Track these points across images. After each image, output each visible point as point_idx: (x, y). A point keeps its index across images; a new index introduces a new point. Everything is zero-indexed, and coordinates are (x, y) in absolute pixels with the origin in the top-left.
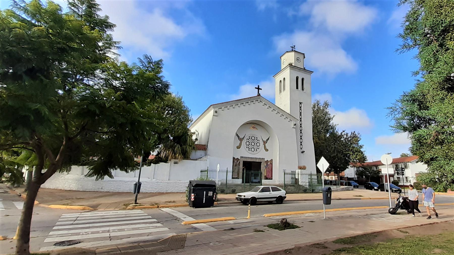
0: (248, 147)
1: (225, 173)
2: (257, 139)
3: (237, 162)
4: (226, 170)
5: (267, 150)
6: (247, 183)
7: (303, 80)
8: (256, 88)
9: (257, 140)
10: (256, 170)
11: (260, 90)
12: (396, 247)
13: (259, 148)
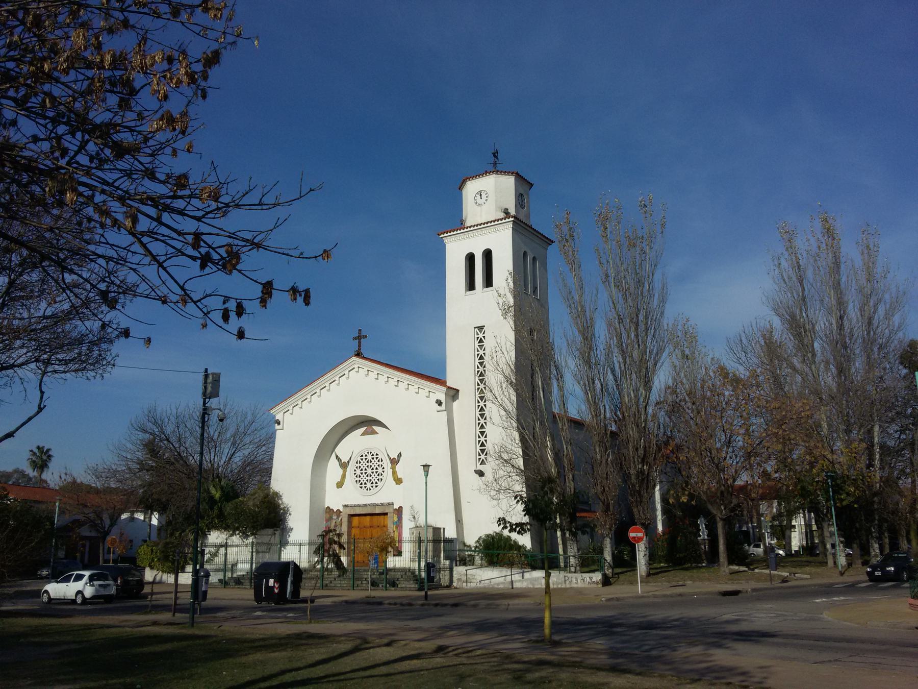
3: (338, 518)
5: (398, 481)
8: (360, 331)
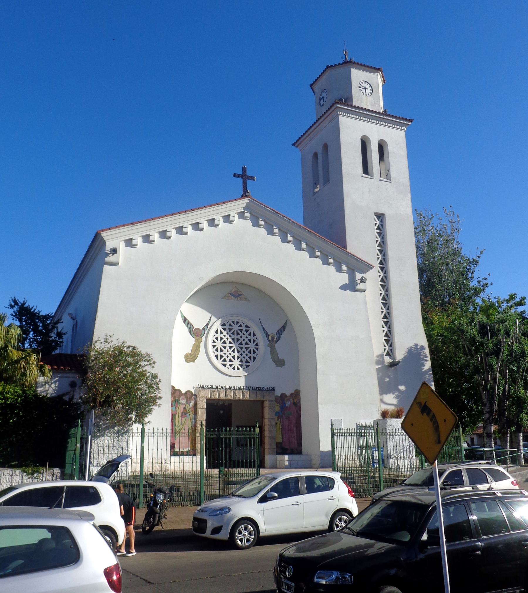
2: (247, 331)
5: (280, 363)
7: (382, 147)
8: (235, 175)
9: (246, 334)
10: (242, 427)
11: (248, 181)
13: (255, 358)
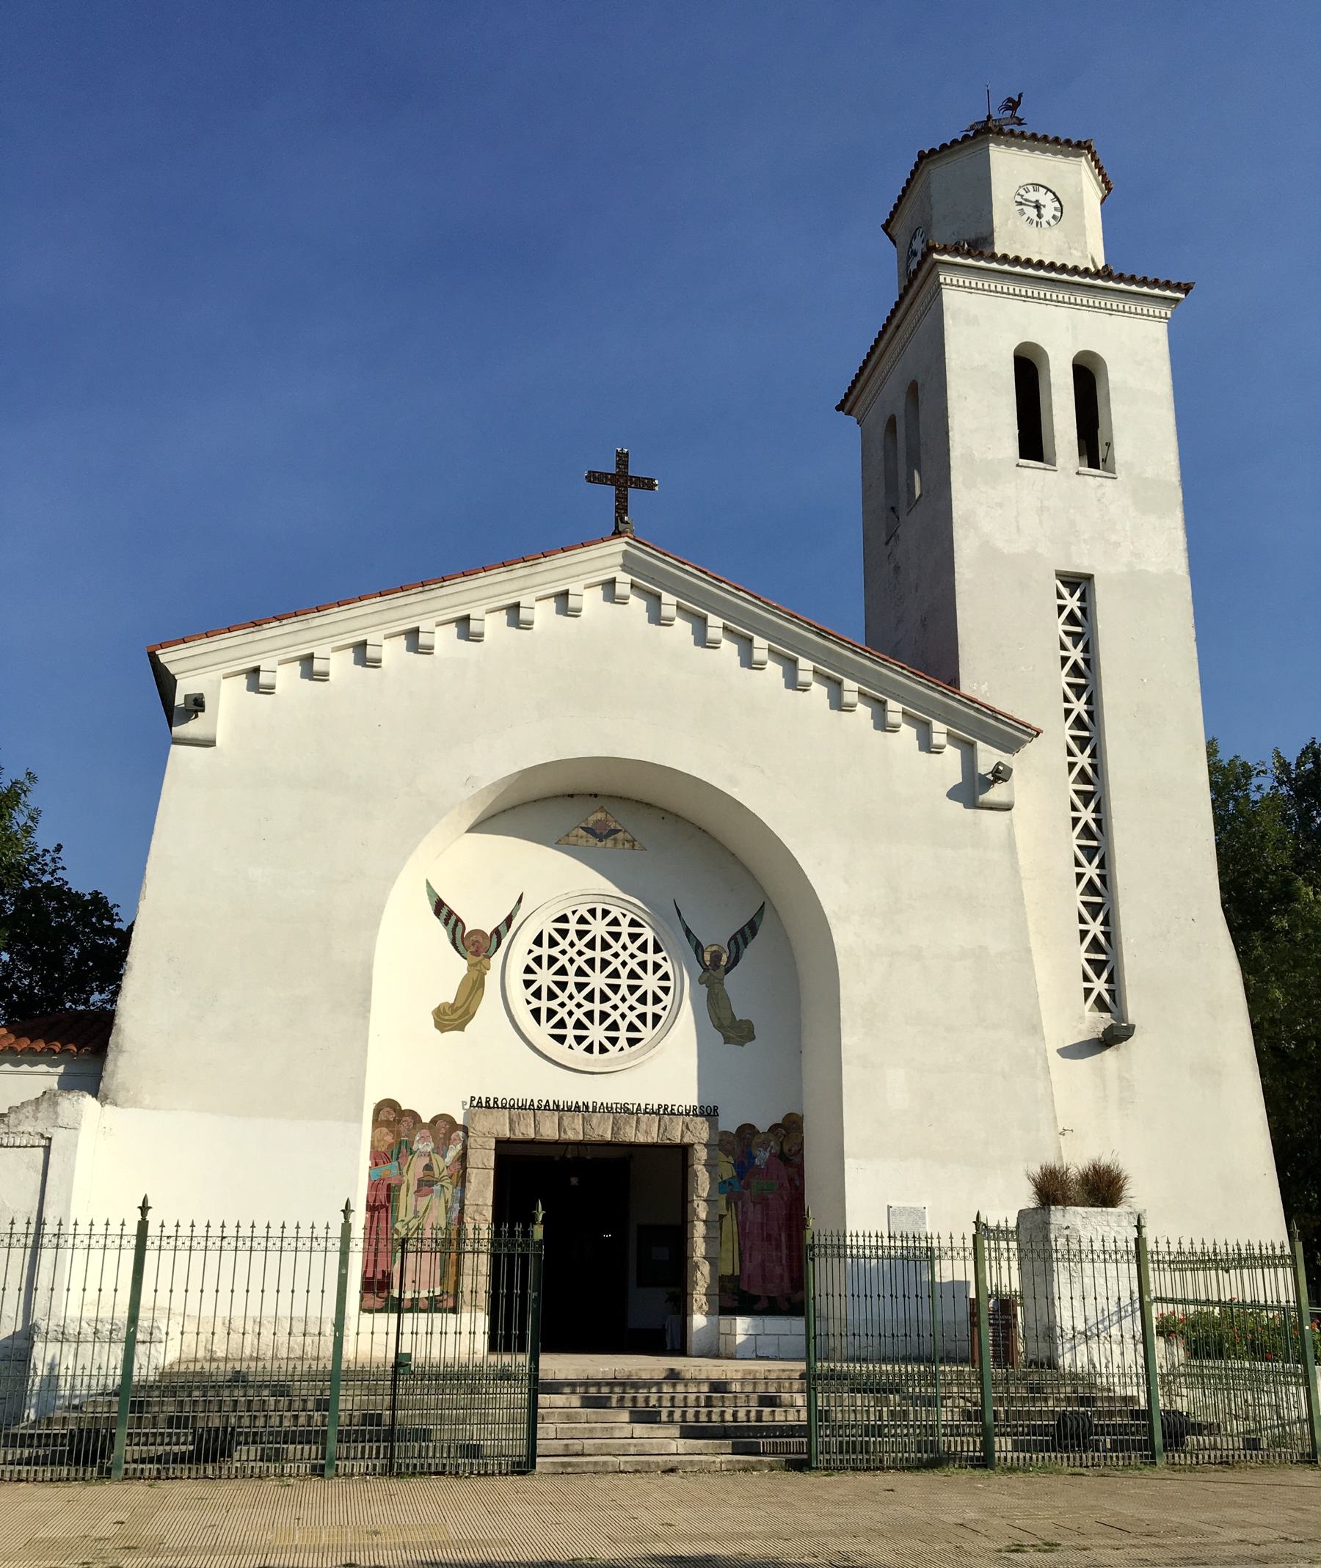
0: (551, 1013)
1: (112, 1255)
3: (441, 1149)
4: (132, 1229)
6: (508, 1349)
12: (1156, 1311)
